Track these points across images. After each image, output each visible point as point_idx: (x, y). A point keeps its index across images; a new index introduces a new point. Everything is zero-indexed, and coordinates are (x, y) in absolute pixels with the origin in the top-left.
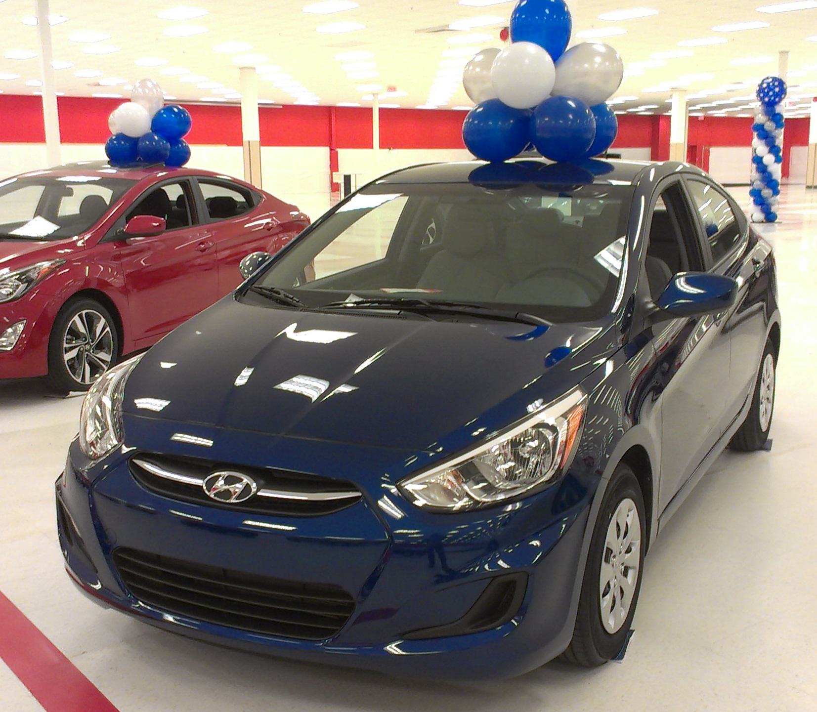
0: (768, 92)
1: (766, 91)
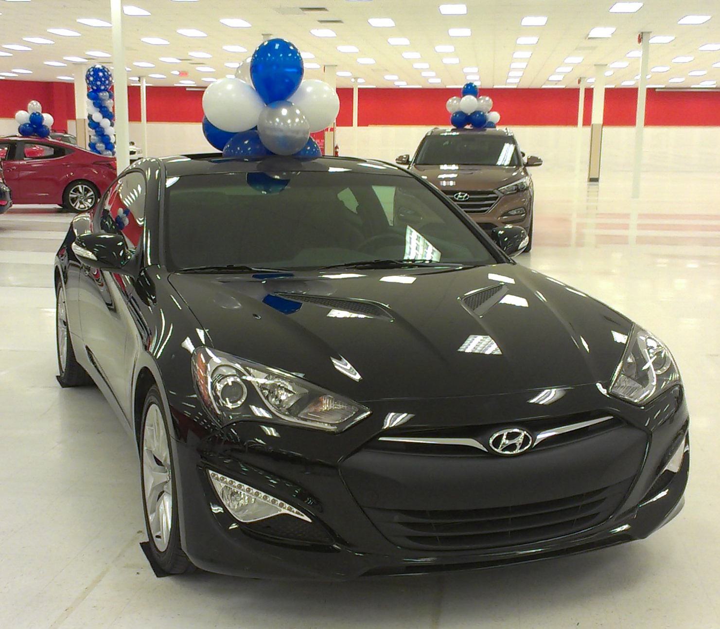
0: (105, 81)
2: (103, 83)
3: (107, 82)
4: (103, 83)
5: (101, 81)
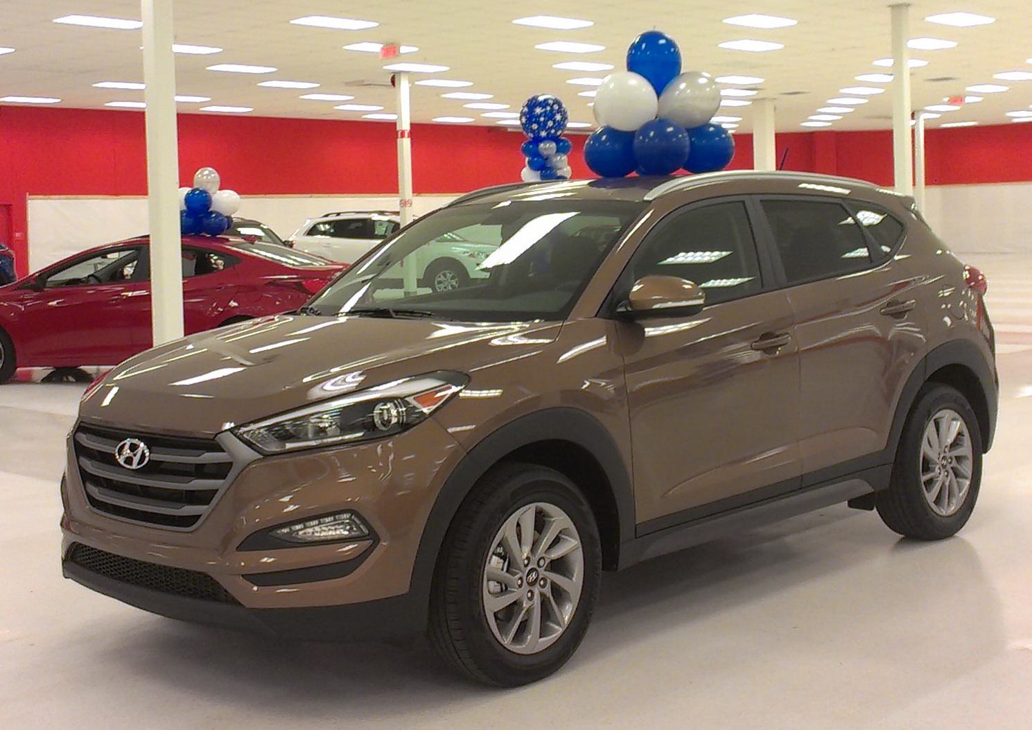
1: (542, 119)
2: (543, 126)
3: (550, 124)
4: (543, 126)
5: (538, 123)
